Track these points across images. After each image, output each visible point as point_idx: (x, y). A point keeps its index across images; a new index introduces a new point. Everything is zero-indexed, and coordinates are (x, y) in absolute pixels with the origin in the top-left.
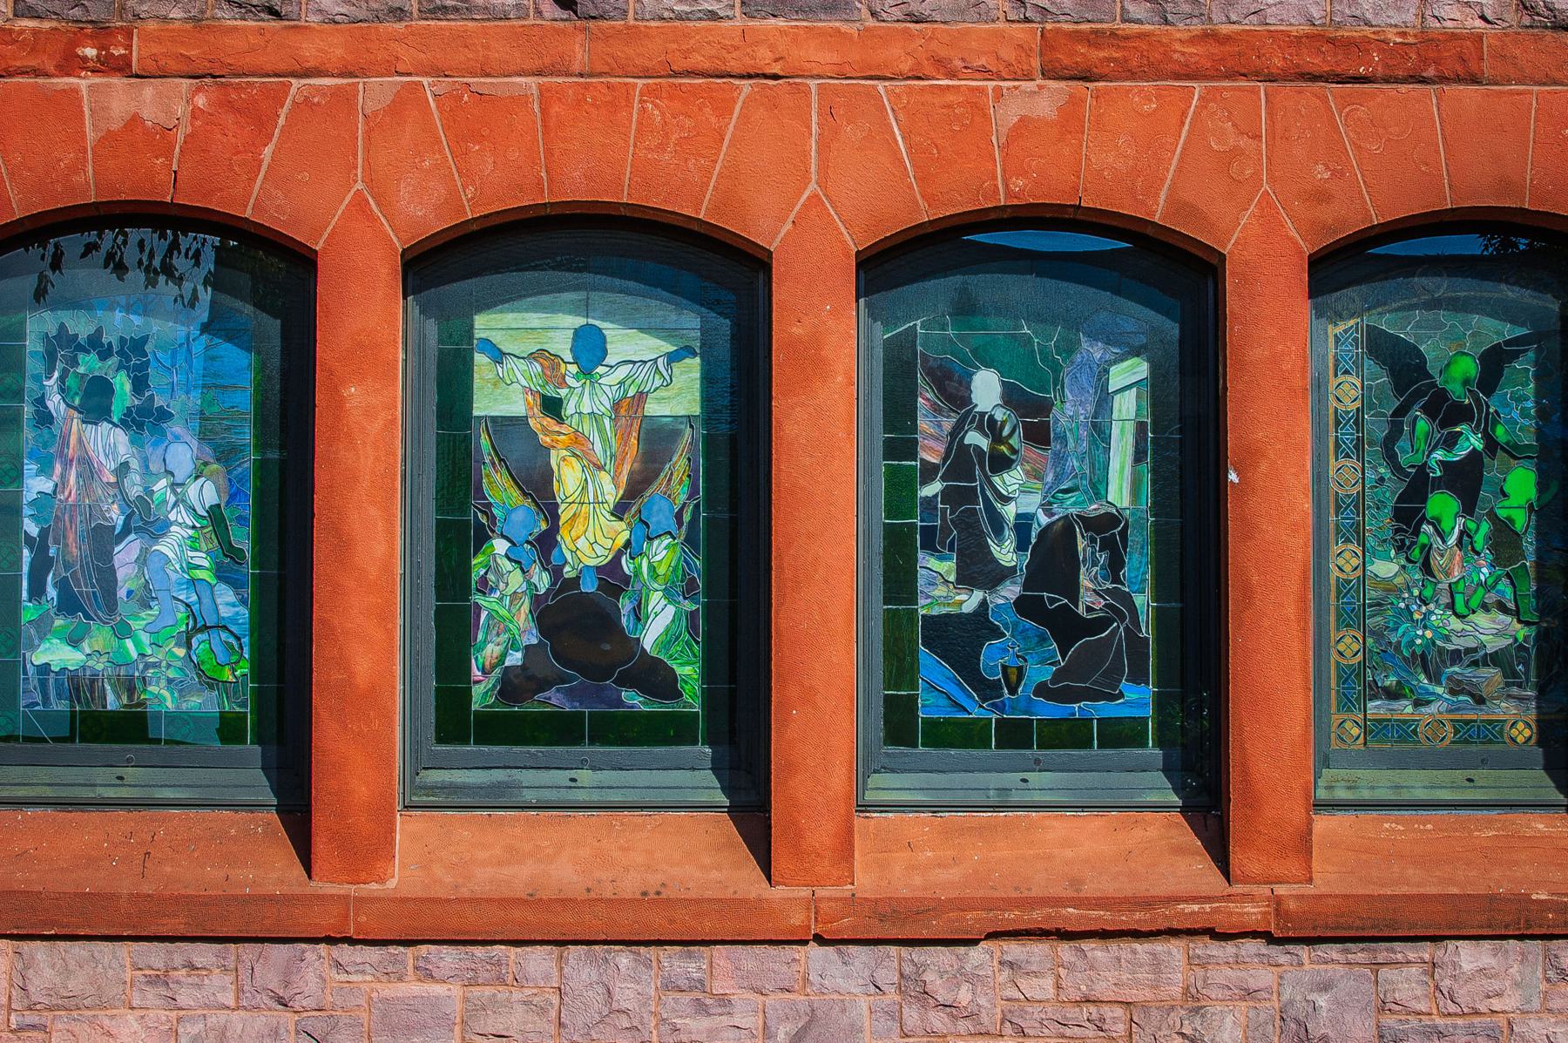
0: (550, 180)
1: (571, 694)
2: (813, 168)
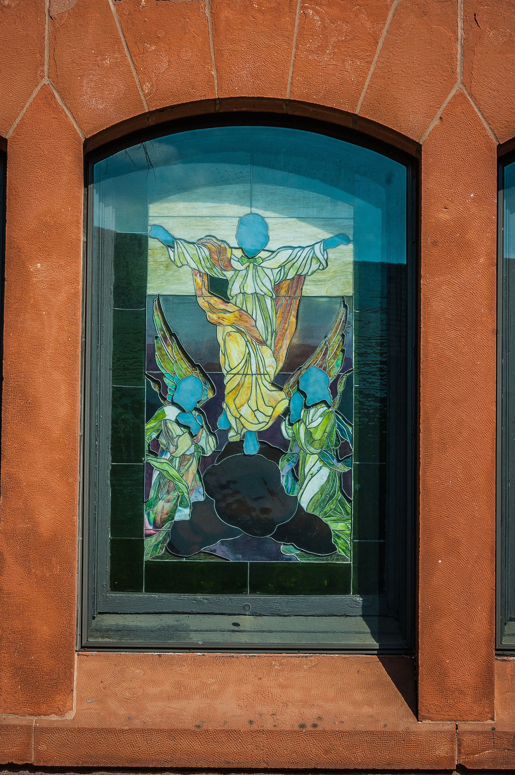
0: (220, 78)
1: (234, 546)
2: (459, 70)
